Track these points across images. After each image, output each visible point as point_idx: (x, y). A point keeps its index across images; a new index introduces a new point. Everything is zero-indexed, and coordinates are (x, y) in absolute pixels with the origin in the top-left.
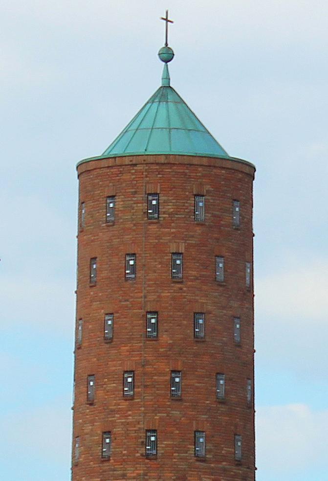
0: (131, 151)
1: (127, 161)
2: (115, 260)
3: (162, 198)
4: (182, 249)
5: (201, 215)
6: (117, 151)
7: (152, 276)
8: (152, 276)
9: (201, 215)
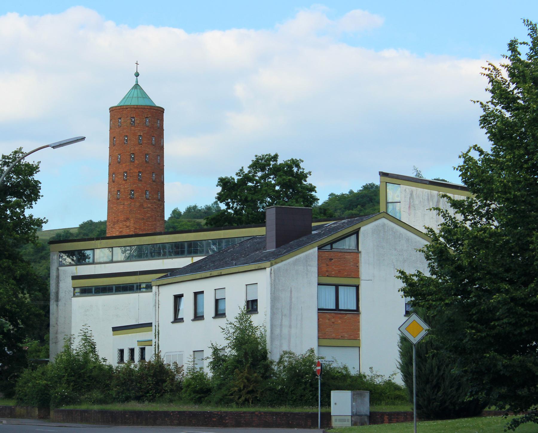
0: (126, 104)
1: (125, 107)
2: (121, 138)
3: (136, 119)
4: (142, 134)
5: (148, 124)
6: (121, 104)
7: (132, 142)
8: (132, 142)
9: (148, 124)
